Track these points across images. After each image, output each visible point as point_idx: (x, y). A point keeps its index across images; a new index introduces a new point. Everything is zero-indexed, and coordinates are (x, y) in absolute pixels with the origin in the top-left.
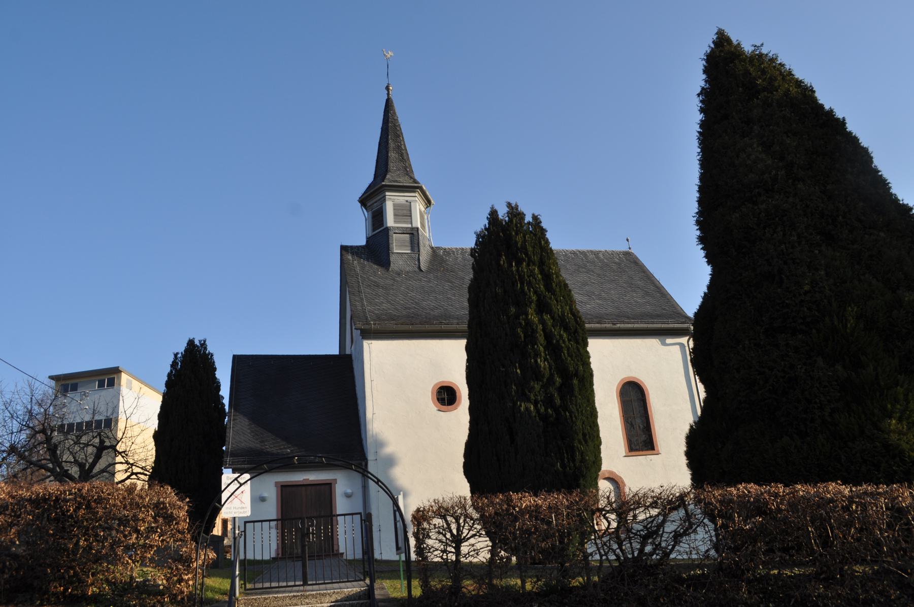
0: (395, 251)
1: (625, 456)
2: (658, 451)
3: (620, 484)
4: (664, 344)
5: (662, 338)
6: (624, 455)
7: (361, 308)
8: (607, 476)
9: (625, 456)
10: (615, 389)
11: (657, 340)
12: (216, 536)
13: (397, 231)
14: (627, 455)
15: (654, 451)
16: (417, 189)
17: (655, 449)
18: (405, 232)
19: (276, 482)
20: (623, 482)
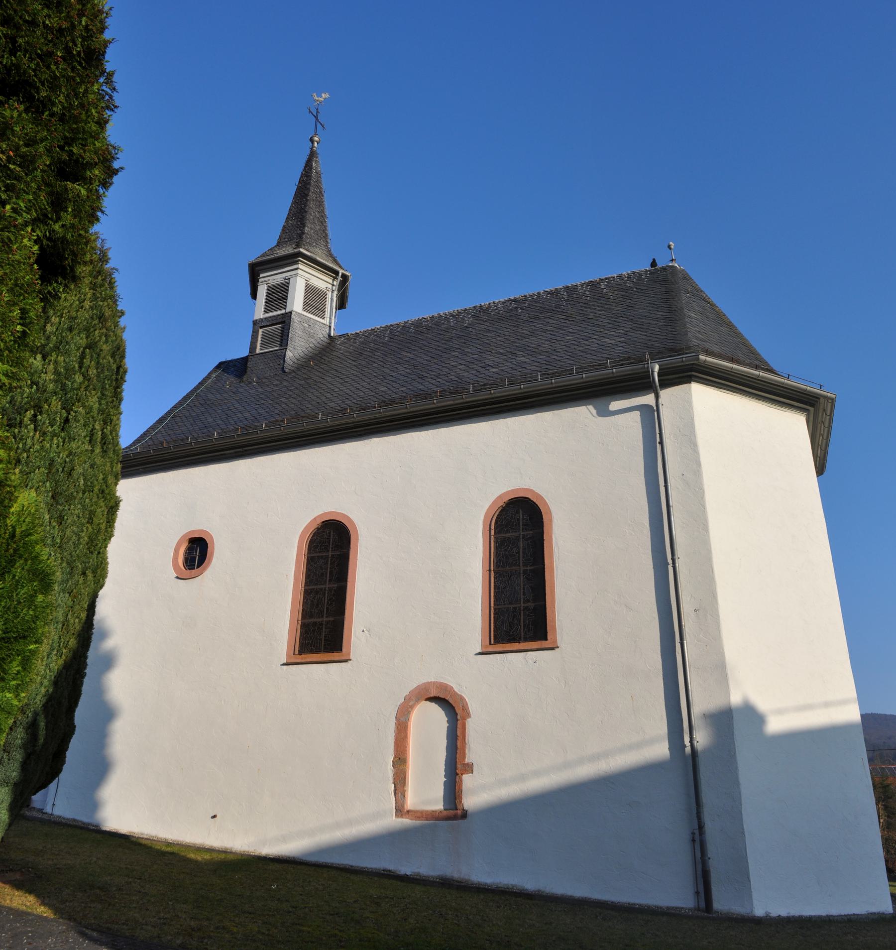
0: (261, 331)
1: (284, 664)
2: (556, 641)
3: (459, 711)
4: (604, 412)
5: (600, 401)
6: (479, 650)
7: (212, 420)
8: (432, 695)
9: (284, 664)
10: (482, 518)
11: (591, 407)
12: (615, 415)
13: (263, 324)
14: (491, 649)
15: (544, 642)
16: (299, 257)
17: (549, 637)
18: (274, 322)
19: (546, 639)
20: (465, 708)
